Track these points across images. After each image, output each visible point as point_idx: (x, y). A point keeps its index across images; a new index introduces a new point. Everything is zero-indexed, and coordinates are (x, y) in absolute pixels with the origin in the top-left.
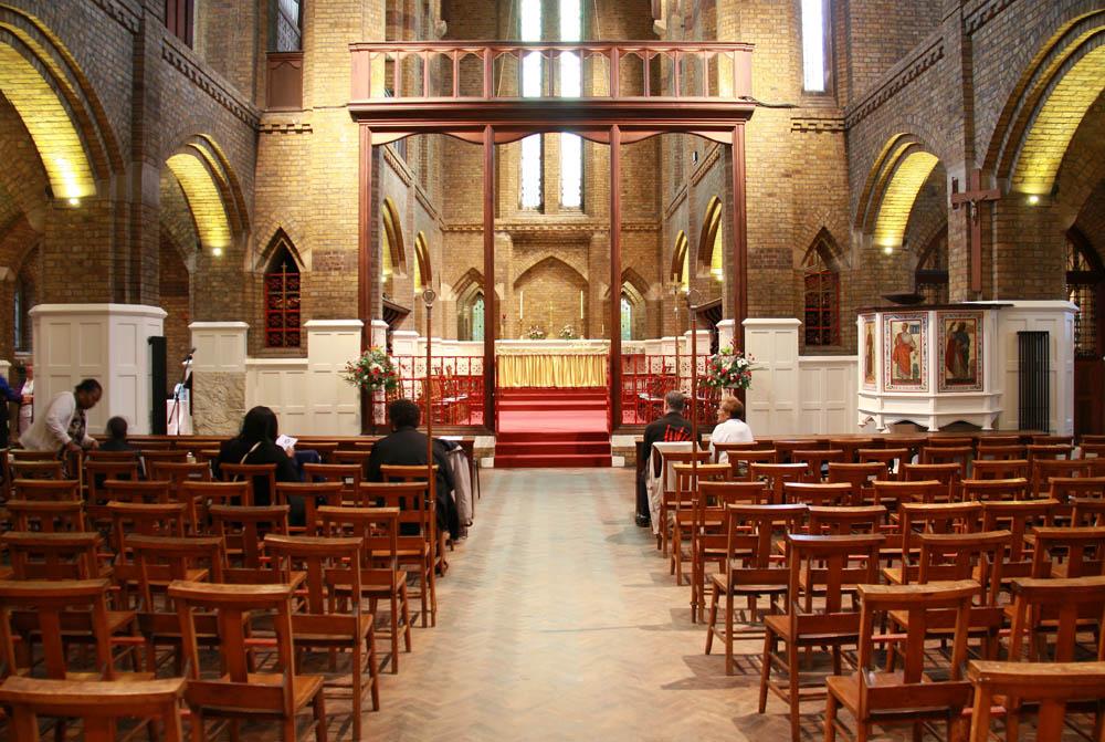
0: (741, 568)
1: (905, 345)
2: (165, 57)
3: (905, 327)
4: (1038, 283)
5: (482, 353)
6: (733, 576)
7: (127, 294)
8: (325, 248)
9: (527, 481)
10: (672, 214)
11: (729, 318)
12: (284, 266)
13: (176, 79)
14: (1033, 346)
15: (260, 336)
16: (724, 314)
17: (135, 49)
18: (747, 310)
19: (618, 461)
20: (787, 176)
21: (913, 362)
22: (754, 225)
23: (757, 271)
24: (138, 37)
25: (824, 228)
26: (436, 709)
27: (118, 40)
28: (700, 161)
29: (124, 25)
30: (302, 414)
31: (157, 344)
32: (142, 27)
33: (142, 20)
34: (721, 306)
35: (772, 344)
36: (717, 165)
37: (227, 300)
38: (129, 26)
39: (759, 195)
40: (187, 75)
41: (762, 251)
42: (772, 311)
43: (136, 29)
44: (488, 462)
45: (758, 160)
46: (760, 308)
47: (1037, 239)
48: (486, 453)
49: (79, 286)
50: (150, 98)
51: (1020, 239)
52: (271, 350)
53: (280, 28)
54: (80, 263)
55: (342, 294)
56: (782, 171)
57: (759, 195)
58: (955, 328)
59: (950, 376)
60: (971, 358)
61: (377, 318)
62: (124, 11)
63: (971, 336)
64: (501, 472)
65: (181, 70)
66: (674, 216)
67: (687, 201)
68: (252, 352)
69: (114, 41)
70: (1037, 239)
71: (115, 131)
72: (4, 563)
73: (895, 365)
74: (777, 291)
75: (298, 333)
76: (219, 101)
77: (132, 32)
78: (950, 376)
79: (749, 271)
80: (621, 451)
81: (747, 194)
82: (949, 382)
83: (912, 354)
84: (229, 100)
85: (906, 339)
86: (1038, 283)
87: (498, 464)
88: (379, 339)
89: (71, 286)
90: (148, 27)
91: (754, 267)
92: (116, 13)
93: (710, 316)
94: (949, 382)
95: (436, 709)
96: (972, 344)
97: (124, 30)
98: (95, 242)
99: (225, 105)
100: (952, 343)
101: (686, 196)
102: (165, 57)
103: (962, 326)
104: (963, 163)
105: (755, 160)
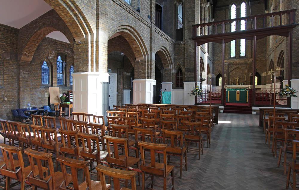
0: (220, 106)
2: (156, 32)
5: (221, 88)
6: (286, 148)
7: (149, 77)
8: (188, 67)
9: (231, 116)
10: (269, 56)
11: (286, 79)
12: (180, 71)
13: (158, 36)
15: (175, 86)
16: (285, 78)
17: (150, 31)
18: (292, 77)
19: (254, 113)
23: (295, 67)
24: (151, 28)
26: (207, 171)
27: (147, 29)
28: (278, 42)
29: (148, 26)
30: (212, 130)
31: (290, 86)
32: (151, 26)
33: (151, 25)
34: (284, 77)
36: (283, 42)
37: (168, 78)
38: (149, 26)
39: (296, 48)
40: (160, 35)
43: (150, 27)
44: (222, 111)
45: (297, 39)
46: (296, 77)
48: (222, 109)
49: (141, 76)
50: (153, 40)
52: (177, 88)
53: (178, 24)
54: (141, 72)
55: (191, 77)
57: (296, 48)
61: (198, 81)
62: (148, 24)
64: (225, 114)
65: (159, 34)
66: (270, 56)
67: (274, 52)
68: (174, 88)
69: (146, 30)
71: (147, 47)
72: (120, 189)
75: (182, 85)
76: (166, 40)
77: (150, 27)
79: (293, 68)
80: (255, 111)
81: (293, 48)
84: (168, 39)
87: (224, 112)
88: (198, 85)
89: (139, 76)
90: (152, 26)
92: (146, 24)
93: (281, 79)
95: (207, 171)
97: (148, 27)
98: (143, 68)
99: (168, 41)
101: (274, 51)
102: (156, 32)
105: (296, 39)
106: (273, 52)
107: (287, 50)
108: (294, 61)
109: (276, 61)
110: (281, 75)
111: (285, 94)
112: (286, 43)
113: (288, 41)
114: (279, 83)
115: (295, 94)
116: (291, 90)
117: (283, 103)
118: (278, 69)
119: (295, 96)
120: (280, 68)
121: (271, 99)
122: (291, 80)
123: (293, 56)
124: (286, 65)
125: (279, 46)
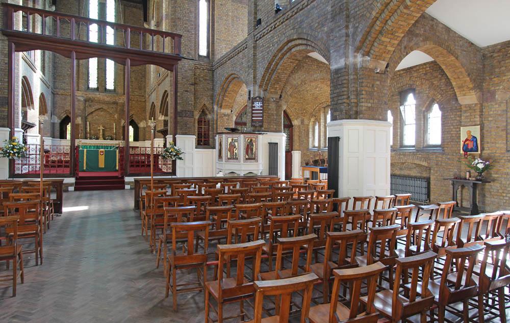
1: (232, 146)
3: (232, 140)
4: (275, 127)
14: (273, 147)
20: (192, 85)
21: (235, 152)
22: (180, 102)
25: (204, 104)
35: (186, 143)
41: (183, 111)
42: (186, 133)
47: (275, 112)
51: (270, 112)
56: (191, 83)
58: (249, 141)
59: (247, 157)
60: (254, 151)
63: (254, 144)
70: (275, 112)
73: (229, 153)
74: (188, 126)
78: (247, 157)
82: (246, 159)
83: (235, 149)
85: (233, 144)
86: (275, 127)
91: (180, 117)
94: (246, 159)
96: (254, 146)
100: (248, 145)
103: (251, 140)
104: (252, 85)
106: (154, 90)
107: (171, 91)
108: (179, 108)
109: (158, 105)
110: (164, 127)
111: (169, 157)
112: (171, 80)
113: (172, 78)
114: (163, 139)
115: (180, 156)
116: (176, 150)
117: (22, 171)
118: (162, 118)
119: (180, 159)
120: (163, 116)
121: (215, 119)
122: (177, 136)
123: (178, 101)
124: (171, 113)
125: (163, 83)
